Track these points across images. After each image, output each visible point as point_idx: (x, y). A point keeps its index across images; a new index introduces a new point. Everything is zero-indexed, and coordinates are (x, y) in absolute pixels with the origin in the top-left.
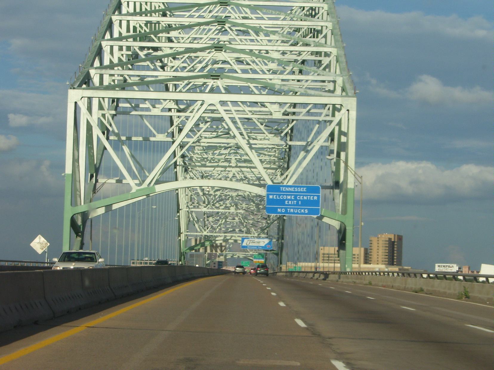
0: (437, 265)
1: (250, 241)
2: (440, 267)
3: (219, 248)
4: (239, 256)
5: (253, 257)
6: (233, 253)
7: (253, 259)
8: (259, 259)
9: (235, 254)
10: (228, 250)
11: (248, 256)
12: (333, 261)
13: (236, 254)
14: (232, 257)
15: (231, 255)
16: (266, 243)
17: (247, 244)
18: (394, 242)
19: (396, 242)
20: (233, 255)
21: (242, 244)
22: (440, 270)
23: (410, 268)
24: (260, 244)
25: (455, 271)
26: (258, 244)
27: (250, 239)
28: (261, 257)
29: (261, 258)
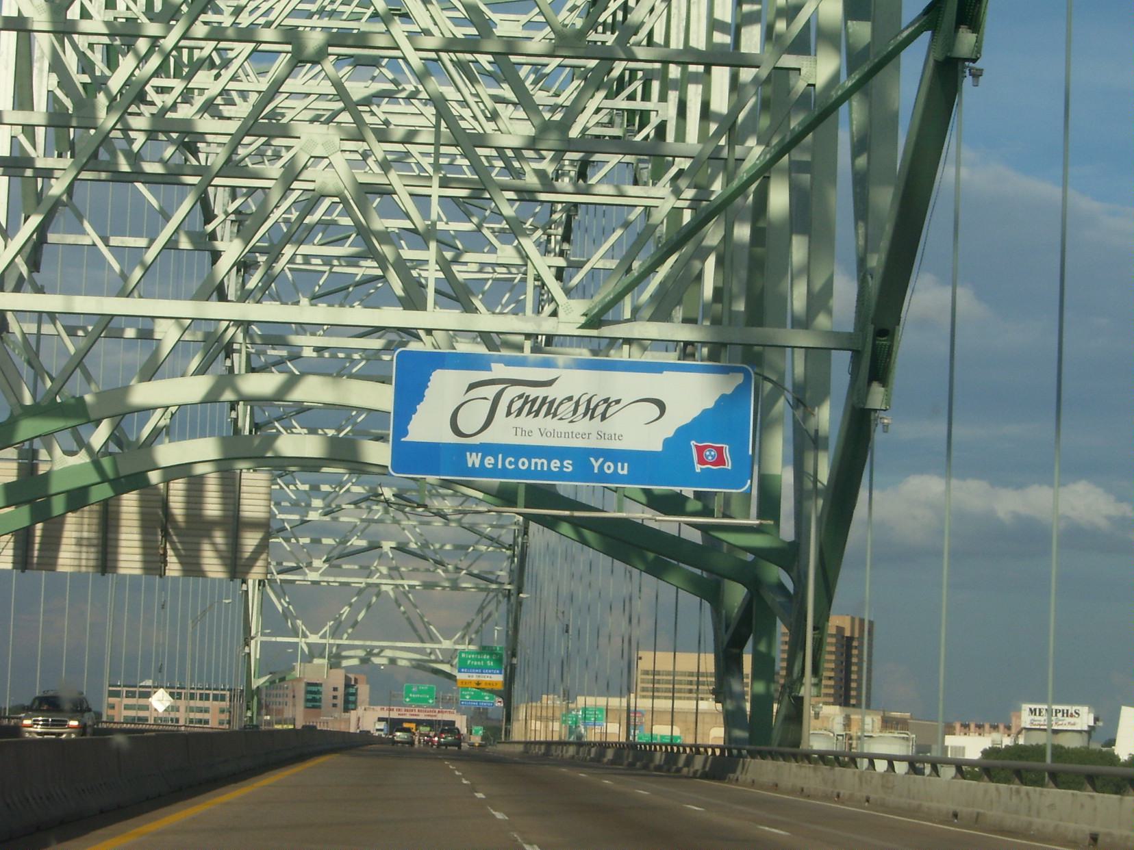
0: (1026, 707)
1: (491, 391)
2: (1037, 713)
3: (219, 537)
4: (393, 661)
5: (456, 661)
6: (368, 643)
7: (455, 672)
8: (481, 670)
9: (376, 651)
10: (350, 631)
11: (433, 657)
12: (656, 694)
13: (382, 649)
14: (364, 661)
15: (362, 653)
16: (686, 419)
17: (458, 432)
18: (851, 639)
19: (858, 638)
20: (370, 653)
21: (401, 430)
22: (1037, 723)
23: (908, 715)
24: (611, 425)
25: (1086, 728)
26: (583, 425)
27: (499, 371)
28: (492, 664)
29: (490, 668)
